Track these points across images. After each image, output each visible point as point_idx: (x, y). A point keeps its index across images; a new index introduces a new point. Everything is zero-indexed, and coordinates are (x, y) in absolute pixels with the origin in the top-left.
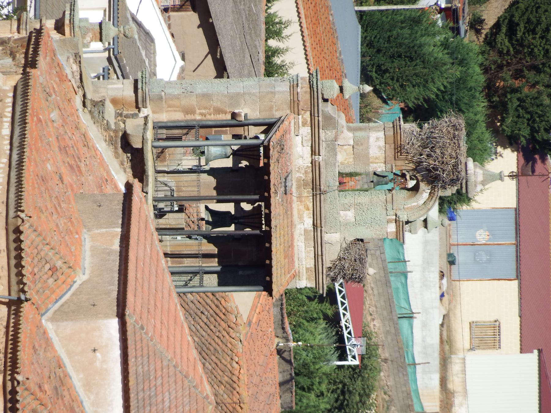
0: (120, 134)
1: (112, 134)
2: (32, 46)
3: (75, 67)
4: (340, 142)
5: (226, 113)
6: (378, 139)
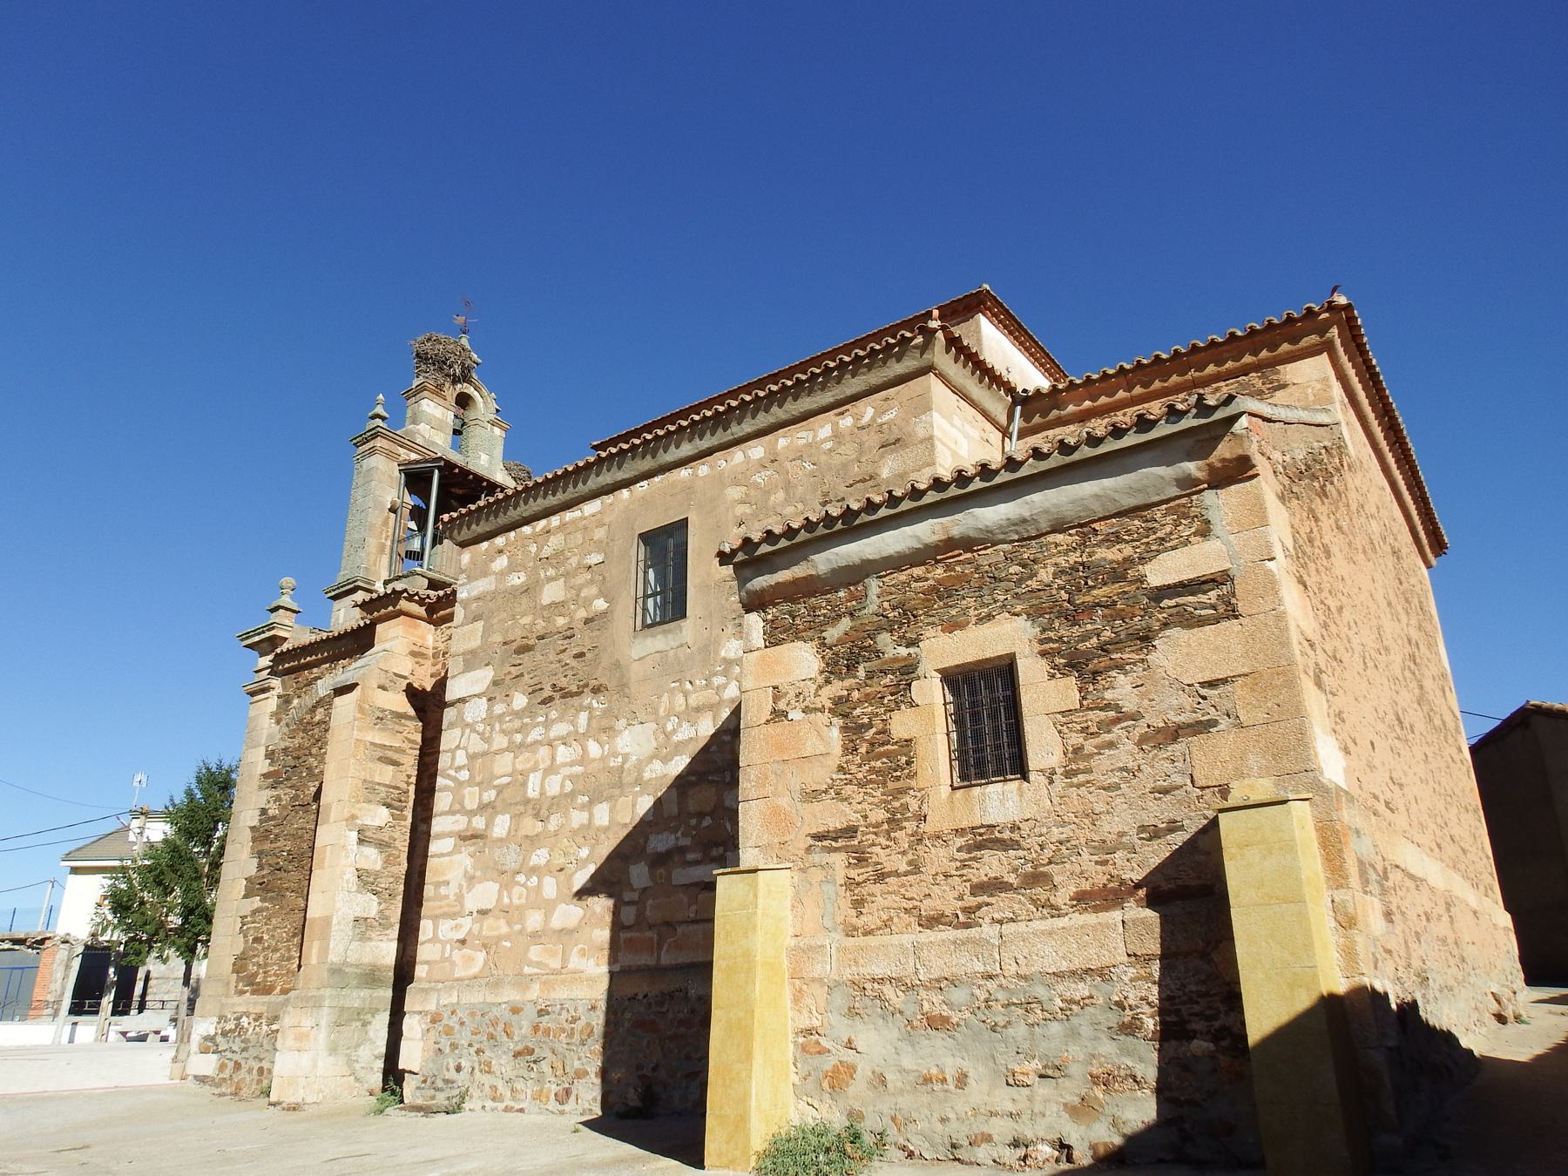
5: (388, 517)
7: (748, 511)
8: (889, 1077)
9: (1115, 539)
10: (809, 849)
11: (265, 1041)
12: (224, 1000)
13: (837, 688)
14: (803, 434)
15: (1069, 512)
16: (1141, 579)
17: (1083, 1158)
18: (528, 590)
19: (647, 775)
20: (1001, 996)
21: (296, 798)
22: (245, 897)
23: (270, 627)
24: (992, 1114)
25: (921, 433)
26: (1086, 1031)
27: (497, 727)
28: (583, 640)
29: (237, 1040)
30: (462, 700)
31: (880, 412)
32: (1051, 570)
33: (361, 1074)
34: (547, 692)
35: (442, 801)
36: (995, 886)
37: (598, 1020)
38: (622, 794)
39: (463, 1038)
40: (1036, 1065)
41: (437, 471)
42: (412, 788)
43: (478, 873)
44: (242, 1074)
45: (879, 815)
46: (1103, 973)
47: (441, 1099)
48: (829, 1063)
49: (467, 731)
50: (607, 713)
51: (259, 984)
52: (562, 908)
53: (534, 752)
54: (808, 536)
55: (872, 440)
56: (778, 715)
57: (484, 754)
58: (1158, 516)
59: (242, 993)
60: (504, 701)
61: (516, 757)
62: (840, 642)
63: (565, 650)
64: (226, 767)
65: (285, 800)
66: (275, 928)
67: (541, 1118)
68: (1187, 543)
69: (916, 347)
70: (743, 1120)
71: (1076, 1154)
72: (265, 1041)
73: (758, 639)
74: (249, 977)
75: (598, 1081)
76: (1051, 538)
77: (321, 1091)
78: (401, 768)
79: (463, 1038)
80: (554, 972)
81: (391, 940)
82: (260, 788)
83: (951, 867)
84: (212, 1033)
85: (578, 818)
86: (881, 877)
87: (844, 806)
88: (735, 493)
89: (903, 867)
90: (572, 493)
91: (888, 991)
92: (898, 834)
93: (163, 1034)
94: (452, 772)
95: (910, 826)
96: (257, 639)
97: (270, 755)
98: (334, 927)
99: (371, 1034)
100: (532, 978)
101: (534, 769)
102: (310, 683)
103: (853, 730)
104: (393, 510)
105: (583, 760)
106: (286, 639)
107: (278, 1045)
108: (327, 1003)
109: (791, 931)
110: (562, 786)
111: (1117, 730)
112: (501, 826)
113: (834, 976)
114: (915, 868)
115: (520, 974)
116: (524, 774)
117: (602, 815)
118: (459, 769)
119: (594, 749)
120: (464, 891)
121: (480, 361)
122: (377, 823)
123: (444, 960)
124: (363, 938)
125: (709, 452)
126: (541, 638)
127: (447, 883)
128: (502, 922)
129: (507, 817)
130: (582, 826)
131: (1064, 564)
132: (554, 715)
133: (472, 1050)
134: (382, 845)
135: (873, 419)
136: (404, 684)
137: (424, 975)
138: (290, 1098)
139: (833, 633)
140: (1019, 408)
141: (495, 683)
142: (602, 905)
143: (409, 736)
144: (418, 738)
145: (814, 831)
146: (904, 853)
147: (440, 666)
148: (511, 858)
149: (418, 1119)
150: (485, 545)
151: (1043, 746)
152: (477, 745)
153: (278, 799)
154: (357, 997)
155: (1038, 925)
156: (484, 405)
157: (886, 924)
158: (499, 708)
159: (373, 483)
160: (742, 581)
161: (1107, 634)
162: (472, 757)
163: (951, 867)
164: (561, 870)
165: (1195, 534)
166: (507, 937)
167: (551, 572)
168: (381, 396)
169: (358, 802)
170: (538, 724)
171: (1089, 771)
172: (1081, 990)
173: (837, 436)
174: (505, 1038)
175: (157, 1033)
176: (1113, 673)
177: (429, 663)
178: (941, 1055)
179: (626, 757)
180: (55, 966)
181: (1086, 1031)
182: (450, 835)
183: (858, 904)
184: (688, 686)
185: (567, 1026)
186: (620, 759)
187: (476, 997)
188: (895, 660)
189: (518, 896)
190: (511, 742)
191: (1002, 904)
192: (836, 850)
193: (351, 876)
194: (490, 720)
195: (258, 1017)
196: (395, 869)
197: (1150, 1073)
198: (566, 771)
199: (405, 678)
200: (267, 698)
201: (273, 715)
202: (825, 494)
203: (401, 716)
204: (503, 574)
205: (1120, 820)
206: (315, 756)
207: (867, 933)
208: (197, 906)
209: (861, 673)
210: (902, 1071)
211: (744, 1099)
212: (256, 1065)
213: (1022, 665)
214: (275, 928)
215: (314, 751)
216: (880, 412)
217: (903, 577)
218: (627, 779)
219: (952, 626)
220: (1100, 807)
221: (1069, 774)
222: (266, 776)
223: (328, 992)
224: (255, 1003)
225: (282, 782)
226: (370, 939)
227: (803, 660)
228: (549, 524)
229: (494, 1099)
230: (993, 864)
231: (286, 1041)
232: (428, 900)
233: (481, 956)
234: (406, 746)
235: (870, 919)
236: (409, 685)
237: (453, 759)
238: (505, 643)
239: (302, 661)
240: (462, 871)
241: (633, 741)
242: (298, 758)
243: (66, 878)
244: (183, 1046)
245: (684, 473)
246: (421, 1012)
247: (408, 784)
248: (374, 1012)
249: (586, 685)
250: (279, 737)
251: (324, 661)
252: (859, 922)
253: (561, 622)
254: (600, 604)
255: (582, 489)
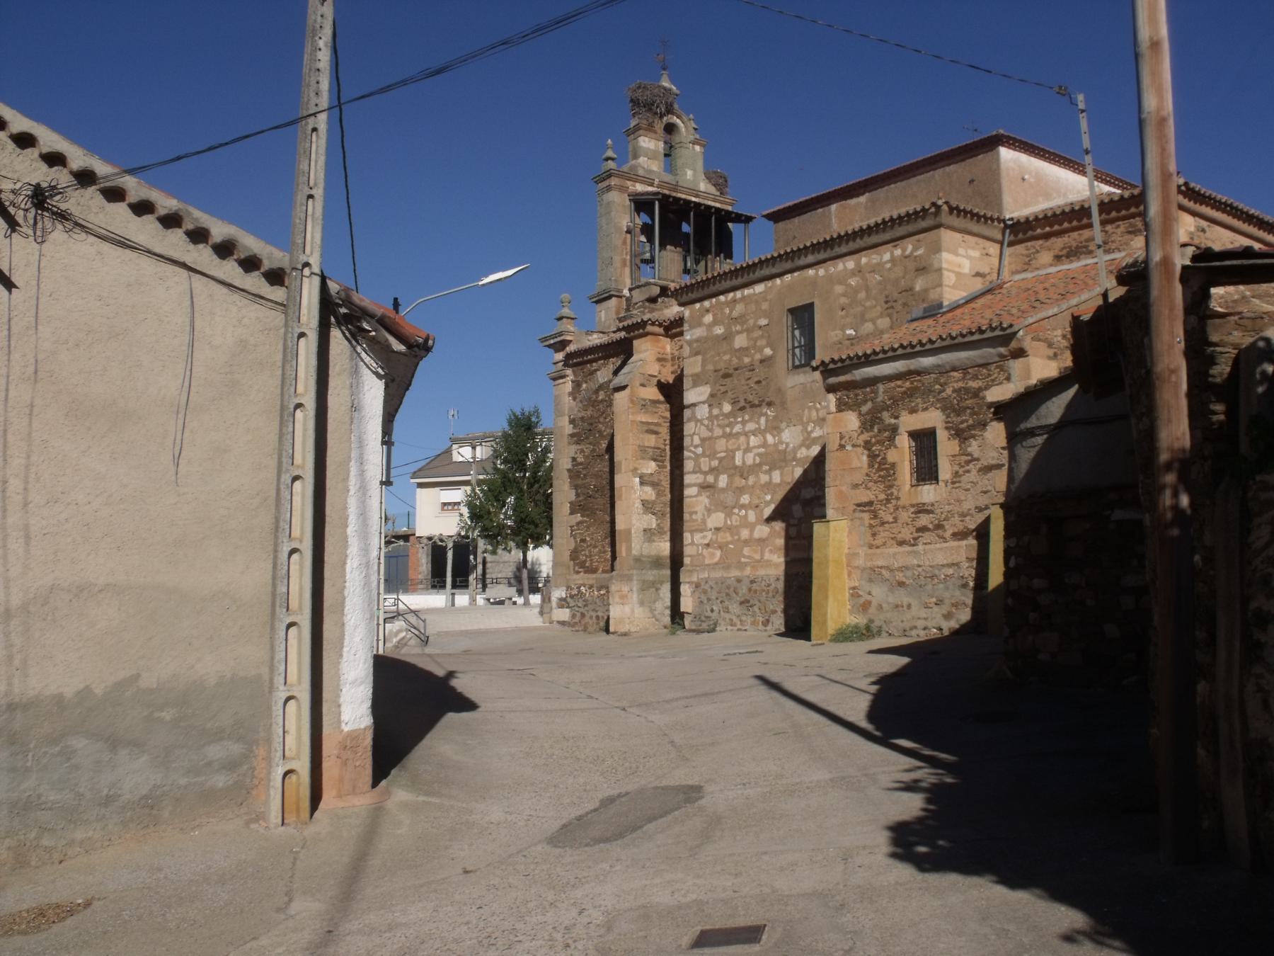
0: (647, 304)
1: (646, 311)
2: (585, 358)
3: (595, 336)
4: (646, 166)
5: (626, 238)
6: (644, 141)
7: (847, 302)
8: (884, 606)
9: (975, 377)
10: (854, 511)
11: (598, 600)
12: (568, 577)
13: (866, 436)
14: (874, 256)
15: (957, 364)
16: (984, 398)
17: (946, 633)
18: (727, 337)
19: (799, 455)
20: (923, 574)
21: (594, 450)
22: (571, 514)
23: (560, 334)
24: (919, 618)
25: (936, 265)
26: (951, 587)
27: (715, 423)
28: (760, 372)
29: (580, 600)
30: (694, 405)
31: (915, 249)
32: (951, 389)
33: (658, 617)
34: (742, 403)
35: (689, 465)
36: (923, 529)
37: (781, 585)
38: (786, 466)
39: (713, 595)
40: (934, 600)
41: (657, 202)
42: (668, 448)
43: (713, 507)
44: (587, 619)
45: (882, 496)
46: (957, 565)
47: (705, 626)
48: (861, 601)
49: (699, 424)
50: (775, 417)
51: (588, 567)
52: (758, 527)
53: (738, 439)
54: (850, 362)
55: (911, 265)
56: (842, 447)
57: (710, 438)
58: (993, 369)
59: (578, 572)
60: (718, 407)
61: (727, 441)
62: (867, 413)
63: (749, 379)
64: (527, 414)
65: (587, 452)
66: (593, 534)
67: (755, 633)
68: (1001, 383)
69: (931, 213)
70: (825, 622)
71: (944, 631)
72: (598, 600)
73: (833, 408)
74: (578, 560)
75: (782, 615)
76: (952, 374)
77: (638, 626)
78: (660, 435)
79: (713, 595)
80: (759, 561)
81: (666, 541)
82: (569, 443)
83: (909, 521)
84: (564, 596)
85: (764, 478)
86: (883, 524)
87: (868, 492)
88: (839, 289)
89: (891, 520)
90: (746, 279)
91: (884, 572)
92: (889, 505)
93: (514, 599)
94: (692, 449)
95: (894, 502)
96: (552, 342)
97: (572, 421)
98: (634, 535)
99: (661, 595)
100: (746, 564)
101: (738, 449)
102: (593, 373)
103: (872, 457)
104: (629, 232)
105: (765, 445)
106: (571, 341)
107: (611, 602)
108: (635, 578)
109: (847, 546)
110: (754, 459)
111: (971, 466)
112: (723, 481)
113: (863, 565)
114: (896, 520)
115: (739, 562)
116: (733, 451)
117: (776, 477)
118: (696, 447)
119: (770, 439)
120: (706, 517)
121: (678, 92)
122: (649, 471)
123: (699, 554)
124: (650, 540)
125: (824, 261)
126: (736, 369)
127: (696, 513)
128: (728, 535)
129: (725, 476)
130: (766, 483)
131: (956, 387)
132: (747, 417)
133: (718, 601)
134: (654, 485)
135: (912, 253)
136: (655, 381)
137: (689, 562)
138: (623, 629)
139: (865, 409)
140: (1008, 231)
141: (712, 395)
142: (779, 526)
143: (662, 414)
144: (668, 414)
145: (856, 502)
146: (891, 514)
147: (676, 367)
148: (729, 499)
149: (694, 635)
150: (698, 306)
151: (945, 470)
152: (705, 433)
153: (582, 451)
154: (651, 575)
155: (938, 546)
156: (685, 128)
157: (884, 544)
158: (716, 411)
159: (613, 213)
160: (825, 379)
161: (971, 422)
162: (703, 440)
163: (909, 521)
164: (757, 507)
165: (1005, 379)
166: (731, 543)
167: (738, 328)
168: (609, 141)
169: (637, 459)
170: (738, 423)
171: (959, 482)
172: (950, 571)
173: (893, 260)
174: (734, 595)
175: (510, 599)
176: (971, 440)
177: (669, 364)
178: (902, 597)
179: (787, 444)
180: (420, 555)
181: (951, 587)
182: (694, 485)
183: (874, 535)
184: (818, 406)
185: (765, 588)
186: (784, 446)
187: (718, 574)
188: (889, 425)
189: (735, 521)
190: (724, 432)
191: (927, 536)
192: (863, 511)
193: (638, 504)
194: (711, 418)
195: (591, 587)
196: (663, 499)
197: (969, 602)
198: (756, 451)
199: (655, 376)
200: (565, 383)
201: (570, 394)
202: (887, 297)
203: (655, 402)
204: (710, 326)
205: (968, 505)
206: (603, 424)
207: (878, 547)
208: (527, 517)
209: (876, 430)
210: (889, 603)
211: (825, 614)
212: (594, 615)
213: (938, 432)
214: (593, 534)
215: (601, 420)
216: (915, 249)
217: (893, 385)
218: (789, 457)
219: (913, 411)
220: (963, 498)
221: (953, 483)
222: (572, 436)
223: (635, 572)
224: (588, 579)
225: (581, 441)
226: (654, 541)
227: (852, 421)
228: (735, 296)
229: (732, 625)
230: (924, 520)
231: (614, 600)
232: (687, 521)
233: (718, 553)
234: (661, 421)
235: (878, 542)
236: (659, 382)
237: (692, 440)
238: (716, 371)
239: (585, 358)
240: (703, 505)
241: (790, 436)
242: (592, 424)
243: (414, 494)
244: (545, 605)
245: (811, 272)
246: (689, 583)
247: (665, 445)
248: (662, 583)
249: (763, 401)
250: (576, 409)
251: (600, 359)
252: (874, 543)
253: (747, 360)
254: (768, 351)
255: (752, 276)
